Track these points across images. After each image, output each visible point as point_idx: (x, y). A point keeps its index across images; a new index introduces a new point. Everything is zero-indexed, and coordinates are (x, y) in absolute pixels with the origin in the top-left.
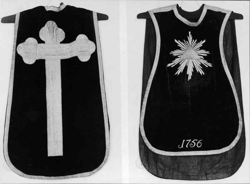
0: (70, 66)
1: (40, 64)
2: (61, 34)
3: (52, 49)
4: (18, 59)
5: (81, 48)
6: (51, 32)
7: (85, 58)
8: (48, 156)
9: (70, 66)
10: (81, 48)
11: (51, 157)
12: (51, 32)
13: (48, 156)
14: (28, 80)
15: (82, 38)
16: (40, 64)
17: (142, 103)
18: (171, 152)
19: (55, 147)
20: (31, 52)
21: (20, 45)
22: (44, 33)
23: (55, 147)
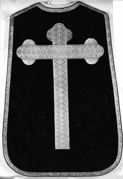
0: (76, 66)
1: (45, 67)
2: (67, 34)
3: (59, 51)
4: (16, 64)
5: (90, 52)
6: (59, 32)
7: (91, 61)
8: (68, 148)
9: (76, 66)
10: (90, 52)
11: (56, 150)
12: (59, 32)
13: (68, 148)
14: (29, 83)
15: (91, 42)
16: (45, 67)
17: (105, 51)
18: (114, 91)
19: (62, 140)
20: (30, 53)
21: (19, 49)
22: (51, 34)
23: (62, 140)
